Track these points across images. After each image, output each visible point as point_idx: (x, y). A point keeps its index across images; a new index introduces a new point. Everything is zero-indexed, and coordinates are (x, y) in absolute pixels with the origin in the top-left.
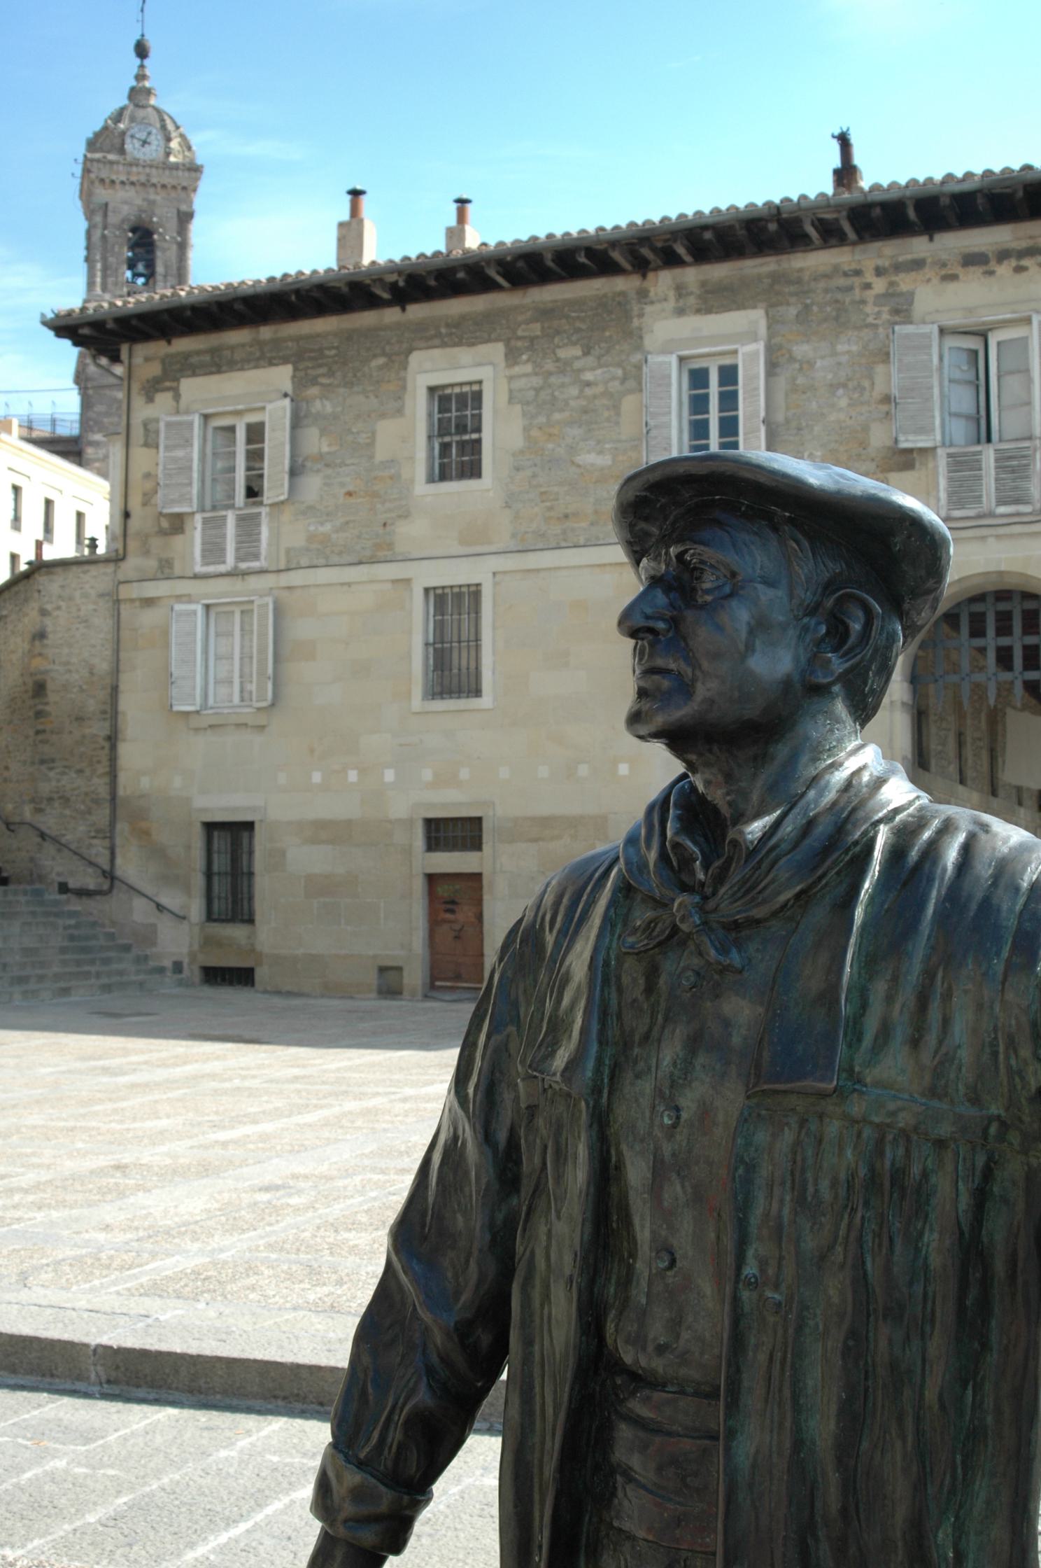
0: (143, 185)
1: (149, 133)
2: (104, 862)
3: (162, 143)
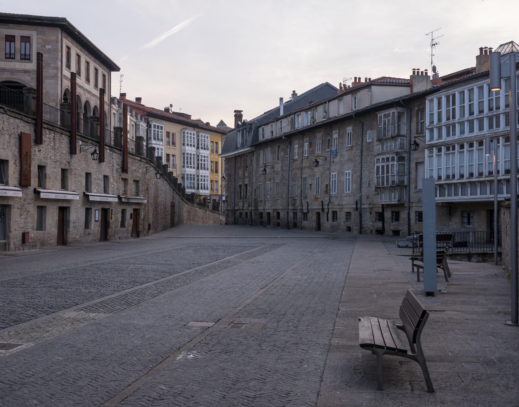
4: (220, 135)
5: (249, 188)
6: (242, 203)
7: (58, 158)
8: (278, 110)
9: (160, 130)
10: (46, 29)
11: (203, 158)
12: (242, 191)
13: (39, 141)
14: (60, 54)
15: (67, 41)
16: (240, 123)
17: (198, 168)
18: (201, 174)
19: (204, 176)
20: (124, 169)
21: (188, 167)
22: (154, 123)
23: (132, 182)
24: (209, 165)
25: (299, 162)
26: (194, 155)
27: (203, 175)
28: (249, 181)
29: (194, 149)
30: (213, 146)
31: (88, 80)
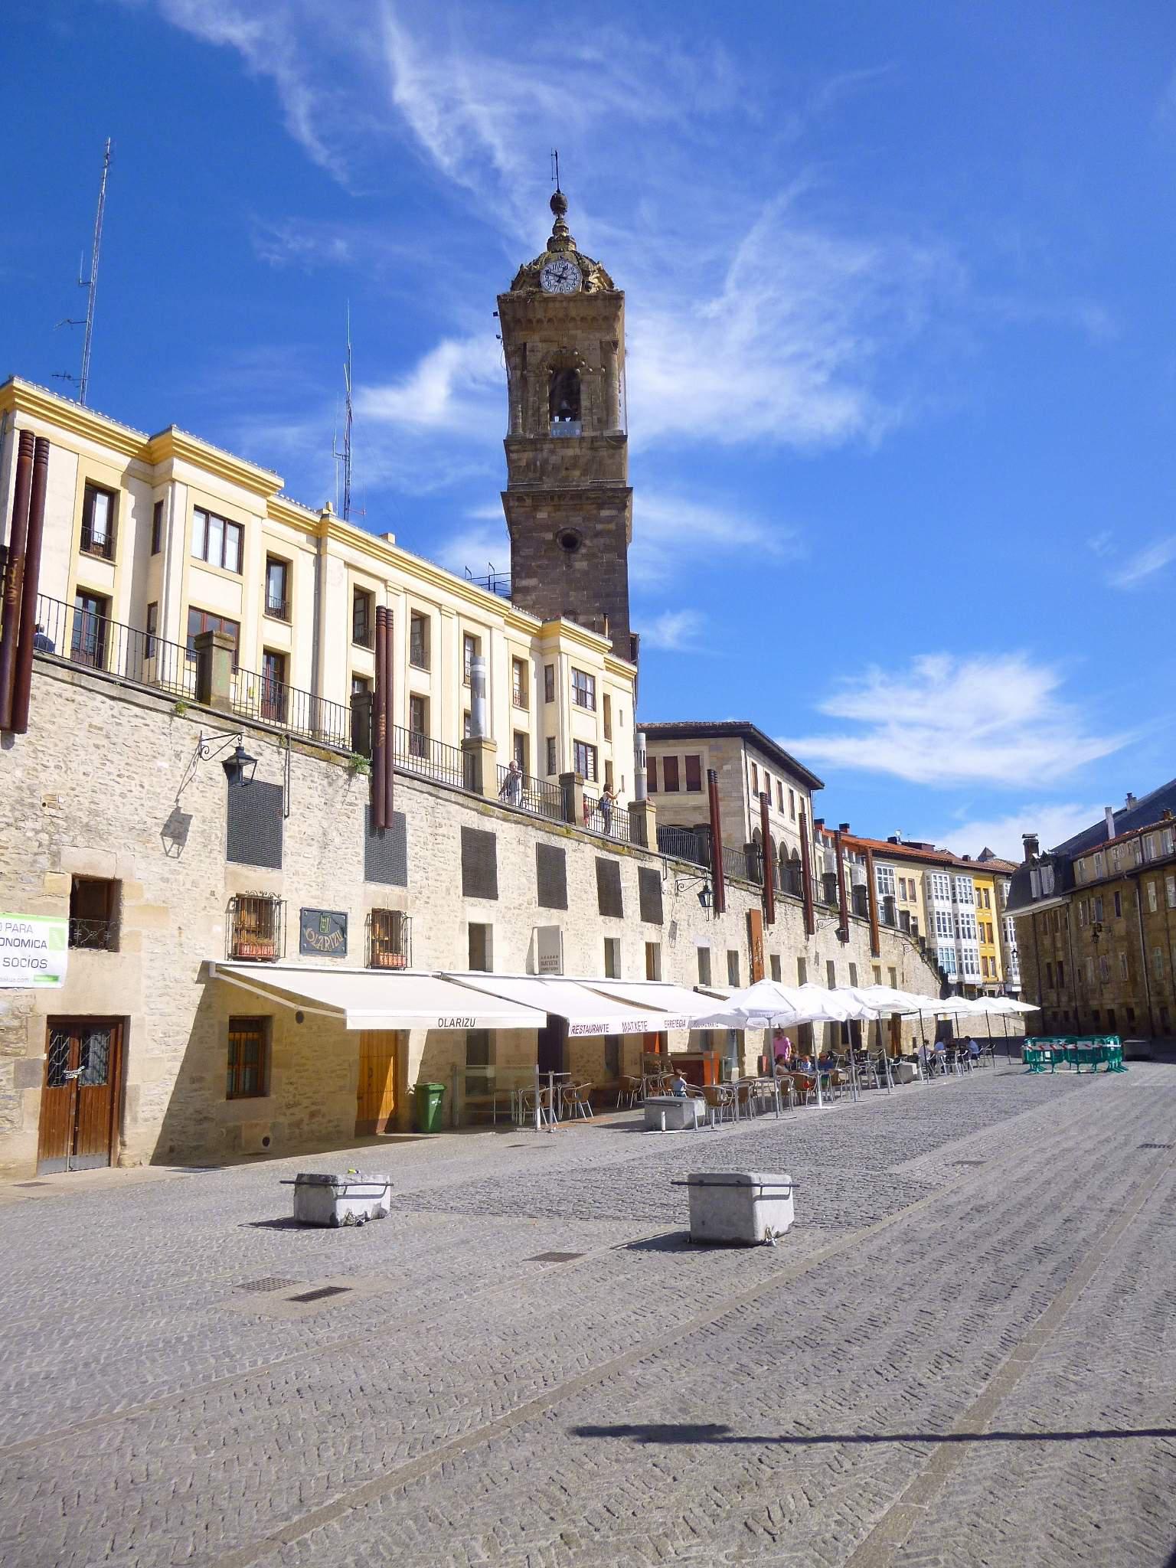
0: (562, 321)
1: (565, 269)
2: (168, 849)
3: (580, 277)
4: (991, 875)
5: (1065, 968)
6: (1055, 995)
7: (792, 942)
8: (1102, 827)
9: (888, 876)
10: (721, 741)
11: (966, 919)
12: (1054, 974)
13: (770, 919)
14: (744, 777)
15: (752, 760)
16: (1035, 855)
17: (958, 937)
18: (964, 947)
19: (971, 950)
20: (875, 951)
21: (940, 935)
22: (878, 864)
23: (887, 970)
24: (975, 929)
25: (1159, 918)
26: (949, 914)
27: (968, 948)
28: (1066, 955)
29: (949, 903)
30: (979, 896)
31: (782, 809)
